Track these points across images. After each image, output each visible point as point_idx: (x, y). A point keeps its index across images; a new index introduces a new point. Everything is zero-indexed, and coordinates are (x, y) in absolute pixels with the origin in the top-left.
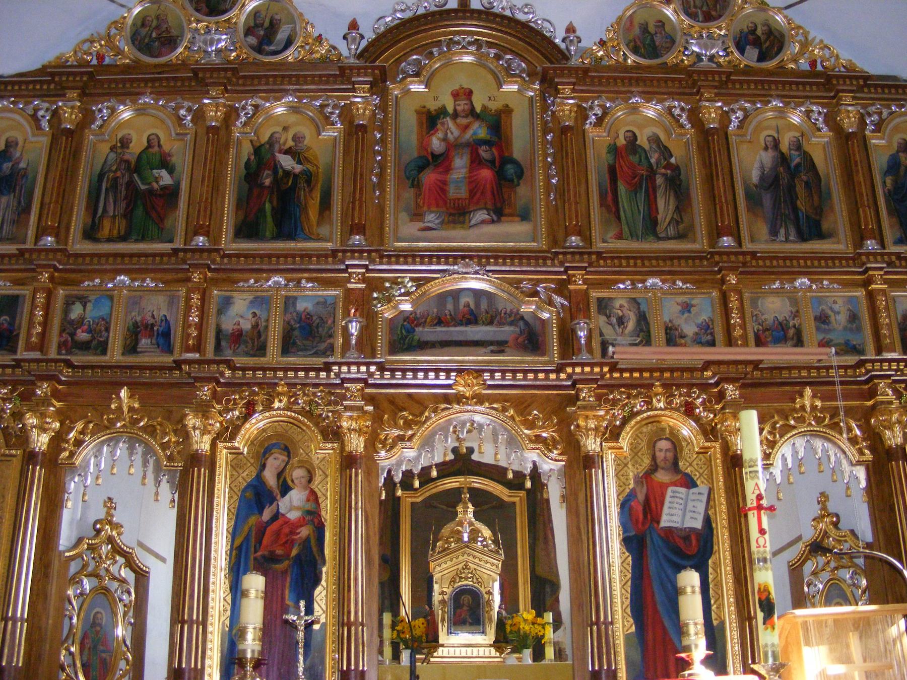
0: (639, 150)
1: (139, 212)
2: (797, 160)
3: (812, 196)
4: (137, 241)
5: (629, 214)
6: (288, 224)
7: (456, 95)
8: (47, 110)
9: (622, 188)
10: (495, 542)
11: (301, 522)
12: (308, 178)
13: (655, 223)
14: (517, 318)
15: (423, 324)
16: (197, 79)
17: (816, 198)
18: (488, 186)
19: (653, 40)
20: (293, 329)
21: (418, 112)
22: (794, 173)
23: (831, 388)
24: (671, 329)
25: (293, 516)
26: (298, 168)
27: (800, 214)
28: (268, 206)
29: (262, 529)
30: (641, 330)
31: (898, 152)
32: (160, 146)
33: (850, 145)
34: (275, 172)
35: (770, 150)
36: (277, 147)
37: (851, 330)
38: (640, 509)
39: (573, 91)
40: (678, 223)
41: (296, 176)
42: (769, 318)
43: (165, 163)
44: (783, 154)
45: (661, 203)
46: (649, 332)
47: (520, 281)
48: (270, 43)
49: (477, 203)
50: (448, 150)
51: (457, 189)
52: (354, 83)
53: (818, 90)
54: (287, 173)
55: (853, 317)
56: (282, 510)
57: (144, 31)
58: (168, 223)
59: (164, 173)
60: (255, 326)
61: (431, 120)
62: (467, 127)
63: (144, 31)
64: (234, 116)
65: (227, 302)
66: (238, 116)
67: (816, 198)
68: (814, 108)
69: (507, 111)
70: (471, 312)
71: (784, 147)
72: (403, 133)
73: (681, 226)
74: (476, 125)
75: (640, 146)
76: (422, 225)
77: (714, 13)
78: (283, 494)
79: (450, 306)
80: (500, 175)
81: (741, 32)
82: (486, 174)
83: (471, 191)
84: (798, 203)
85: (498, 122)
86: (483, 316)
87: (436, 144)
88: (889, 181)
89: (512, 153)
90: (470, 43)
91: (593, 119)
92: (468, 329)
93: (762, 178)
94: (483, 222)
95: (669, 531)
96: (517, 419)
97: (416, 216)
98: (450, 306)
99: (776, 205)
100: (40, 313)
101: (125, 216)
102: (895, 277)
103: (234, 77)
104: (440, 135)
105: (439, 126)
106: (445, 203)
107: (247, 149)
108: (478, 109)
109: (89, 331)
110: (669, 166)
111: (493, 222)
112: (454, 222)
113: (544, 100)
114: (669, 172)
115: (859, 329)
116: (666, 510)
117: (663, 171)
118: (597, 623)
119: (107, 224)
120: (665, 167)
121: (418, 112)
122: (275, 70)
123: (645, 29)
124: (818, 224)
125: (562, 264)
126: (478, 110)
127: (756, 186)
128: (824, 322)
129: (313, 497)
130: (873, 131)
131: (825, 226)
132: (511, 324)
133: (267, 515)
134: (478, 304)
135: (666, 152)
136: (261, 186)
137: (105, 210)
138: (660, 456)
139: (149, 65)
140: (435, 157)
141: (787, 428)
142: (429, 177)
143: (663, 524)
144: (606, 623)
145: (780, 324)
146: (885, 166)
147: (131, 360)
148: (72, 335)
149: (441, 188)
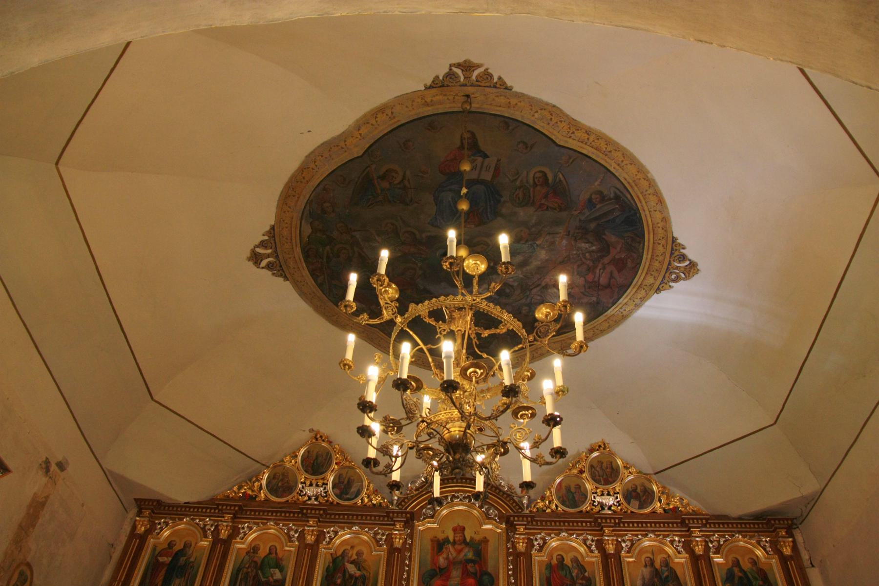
2: (666, 574)
16: (300, 512)
19: (574, 497)
21: (432, 540)
26: (358, 573)
32: (276, 553)
33: (699, 563)
34: (344, 575)
36: (346, 558)
39: (526, 529)
41: (356, 578)
48: (347, 494)
52: (395, 521)
53: (677, 527)
54: (351, 576)
57: (274, 482)
59: (277, 571)
61: (439, 545)
62: (460, 551)
63: (274, 482)
64: (322, 537)
66: (325, 538)
69: (485, 541)
71: (658, 564)
74: (466, 550)
81: (628, 490)
85: (479, 547)
90: (465, 498)
91: (537, 547)
103: (325, 514)
104: (444, 555)
108: (468, 540)
110: (584, 578)
113: (507, 534)
120: (582, 579)
121: (432, 540)
122: (348, 510)
123: (568, 489)
126: (468, 540)
130: (714, 553)
139: (274, 502)
146: (724, 576)
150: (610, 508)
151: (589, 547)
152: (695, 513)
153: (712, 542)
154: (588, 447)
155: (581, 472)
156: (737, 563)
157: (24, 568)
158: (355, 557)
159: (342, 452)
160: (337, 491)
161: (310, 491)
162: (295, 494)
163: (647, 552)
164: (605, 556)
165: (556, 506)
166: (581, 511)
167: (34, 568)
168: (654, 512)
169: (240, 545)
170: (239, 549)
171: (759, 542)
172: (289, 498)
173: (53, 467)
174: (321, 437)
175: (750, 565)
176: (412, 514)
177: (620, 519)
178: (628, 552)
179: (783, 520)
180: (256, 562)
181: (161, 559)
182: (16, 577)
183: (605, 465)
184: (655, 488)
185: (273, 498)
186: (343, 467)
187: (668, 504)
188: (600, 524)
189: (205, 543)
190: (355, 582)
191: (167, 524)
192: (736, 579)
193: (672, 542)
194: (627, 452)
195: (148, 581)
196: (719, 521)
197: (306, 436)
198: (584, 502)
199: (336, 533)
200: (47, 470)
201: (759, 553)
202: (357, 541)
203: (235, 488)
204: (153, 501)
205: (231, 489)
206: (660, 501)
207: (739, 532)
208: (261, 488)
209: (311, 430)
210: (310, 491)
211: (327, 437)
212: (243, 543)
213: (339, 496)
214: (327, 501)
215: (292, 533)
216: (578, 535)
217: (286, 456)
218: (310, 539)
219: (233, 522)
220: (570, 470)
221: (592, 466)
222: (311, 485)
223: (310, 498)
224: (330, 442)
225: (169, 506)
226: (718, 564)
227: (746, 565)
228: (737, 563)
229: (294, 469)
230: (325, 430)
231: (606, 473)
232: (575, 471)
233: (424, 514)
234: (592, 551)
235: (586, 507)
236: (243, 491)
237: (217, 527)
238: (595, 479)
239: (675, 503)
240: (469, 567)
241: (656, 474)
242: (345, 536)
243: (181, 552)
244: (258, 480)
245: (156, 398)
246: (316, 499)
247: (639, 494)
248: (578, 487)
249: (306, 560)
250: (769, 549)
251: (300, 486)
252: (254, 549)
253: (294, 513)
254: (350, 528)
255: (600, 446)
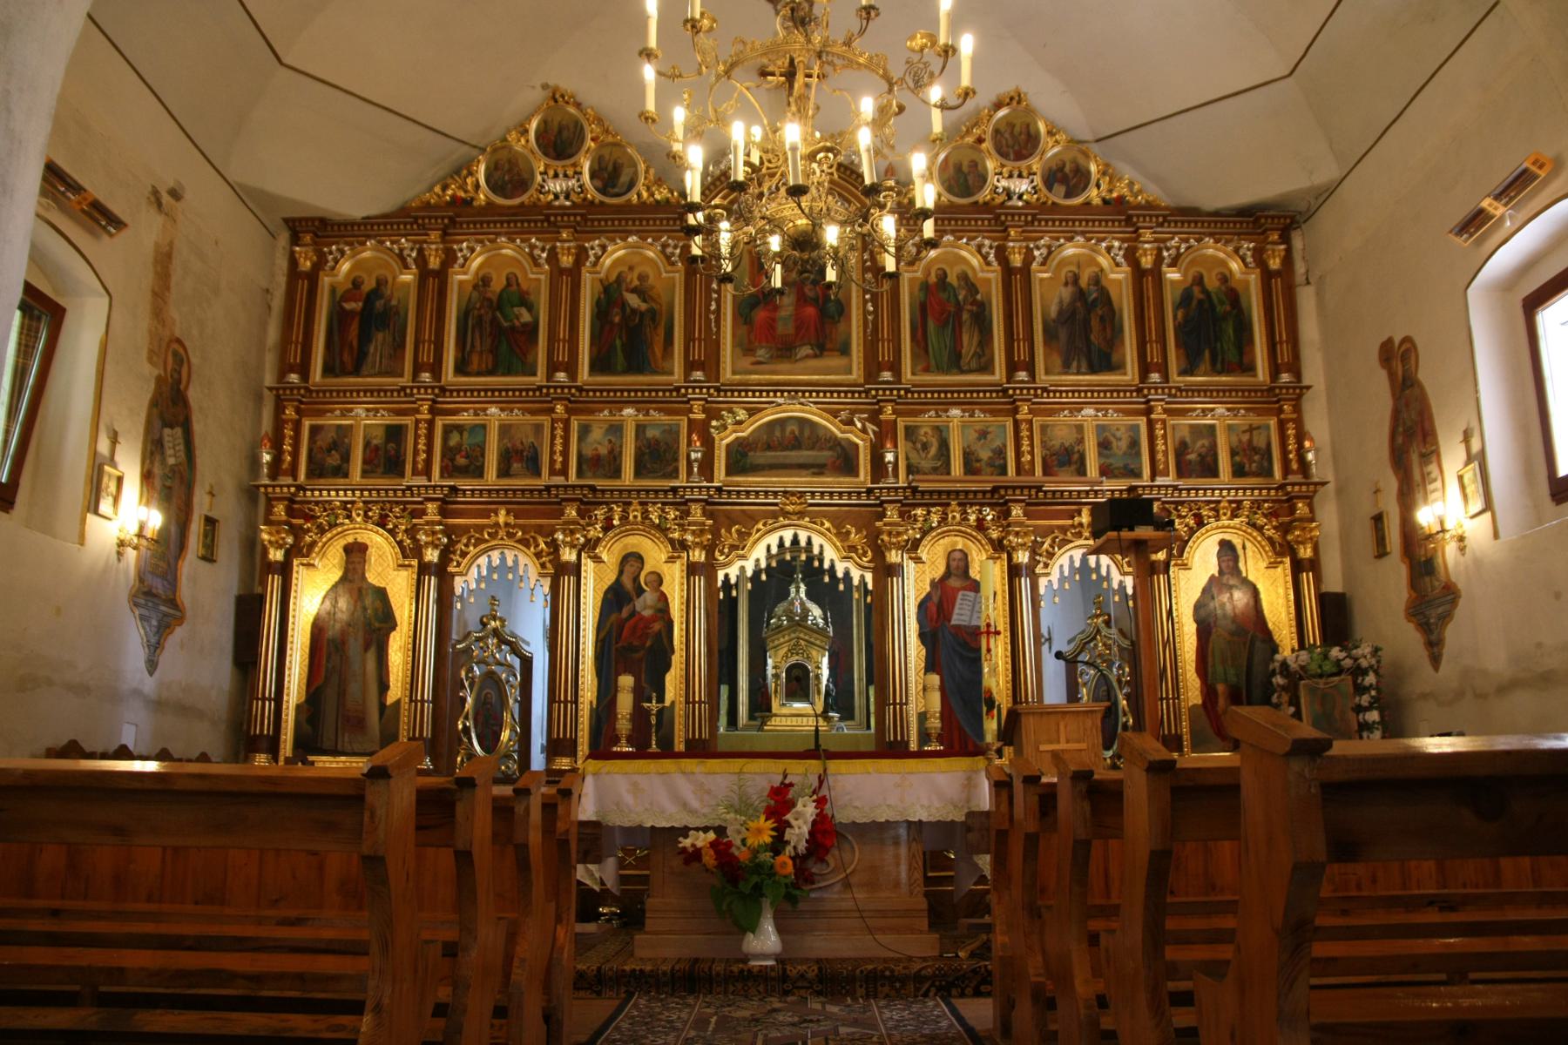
1: (504, 347)
6: (637, 361)
9: (931, 325)
10: (825, 619)
11: (654, 619)
12: (653, 314)
13: (959, 356)
14: (835, 443)
22: (1090, 307)
25: (647, 613)
26: (644, 306)
28: (618, 342)
29: (621, 624)
33: (1145, 280)
38: (934, 609)
41: (642, 314)
43: (525, 301)
45: (965, 338)
47: (839, 411)
48: (614, 186)
51: (785, 327)
54: (634, 311)
56: (638, 608)
57: (497, 175)
58: (530, 358)
59: (524, 311)
60: (611, 452)
65: (585, 431)
66: (588, 257)
70: (796, 438)
71: (1083, 282)
73: (983, 360)
76: (753, 359)
79: (778, 433)
80: (823, 313)
82: (810, 311)
88: (1180, 314)
92: (793, 453)
93: (1060, 313)
94: (807, 356)
95: (958, 627)
98: (778, 433)
100: (422, 441)
103: (588, 219)
109: (467, 457)
110: (975, 302)
111: (816, 356)
116: (956, 611)
118: (895, 704)
119: (475, 359)
123: (958, 168)
131: (1115, 358)
132: (830, 449)
133: (625, 613)
134: (801, 431)
137: (473, 346)
138: (954, 564)
139: (503, 207)
141: (1065, 542)
142: (760, 314)
143: (953, 622)
144: (901, 704)
146: (1178, 300)
147: (506, 483)
148: (452, 460)
149: (771, 324)
150: (1020, 197)
151: (985, 258)
152: (1149, 206)
153: (1168, 249)
154: (994, 99)
155: (980, 140)
156: (1199, 280)
157: (176, 346)
159: (599, 121)
160: (599, 183)
161: (556, 186)
162: (532, 191)
163: (1070, 263)
164: (1008, 271)
166: (976, 203)
167: (187, 344)
168: (1087, 204)
169: (460, 277)
170: (461, 283)
171: (1236, 250)
172: (524, 198)
173: (166, 199)
174: (563, 96)
175: (1217, 284)
177: (1034, 216)
178: (1043, 264)
179: (1279, 218)
180: (489, 300)
181: (348, 306)
182: (170, 360)
183: (1017, 130)
184: (1093, 168)
185: (499, 201)
186: (602, 145)
187: (1110, 191)
188: (1003, 223)
189: (407, 277)
190: (641, 320)
191: (343, 253)
192: (1194, 303)
193: (1109, 249)
194: (1059, 110)
195: (336, 338)
196: (1187, 217)
197: (537, 96)
198: (981, 187)
199: (604, 248)
200: (159, 204)
201: (1235, 266)
202: (636, 259)
203: (437, 189)
204: (313, 219)
205: (430, 189)
206: (1098, 186)
207: (1211, 235)
208: (477, 186)
209: (545, 87)
210: (556, 186)
211: (572, 96)
212: (465, 273)
213: (603, 191)
214: (585, 199)
215: (537, 252)
216: (970, 239)
217: (509, 131)
218: (566, 261)
219: (444, 241)
220: (962, 138)
221: (997, 131)
222: (556, 176)
223: (557, 197)
224: (578, 105)
225: (339, 225)
226: (1173, 282)
227: (1212, 283)
228: (1199, 280)
229: (526, 152)
230: (567, 84)
231: (1017, 142)
232: (970, 140)
234: (988, 264)
235: (984, 195)
236: (450, 192)
237: (421, 251)
238: (1002, 153)
239: (1122, 189)
241: (1098, 141)
242: (616, 252)
243: (376, 293)
244: (470, 173)
245: (286, 60)
246: (567, 197)
247: (1067, 176)
248: (974, 165)
249: (565, 292)
250: (1249, 260)
251: (539, 178)
252: (483, 281)
253: (536, 222)
254: (624, 239)
255: (1012, 99)
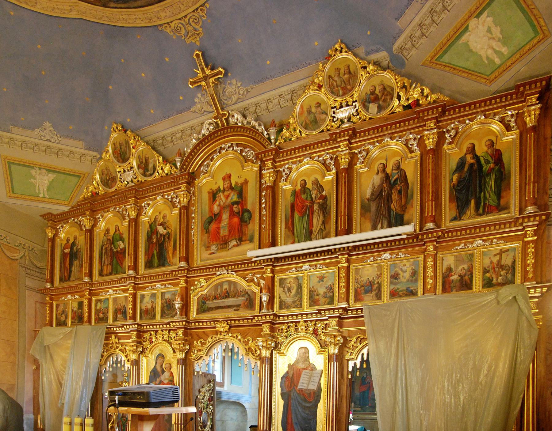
0: (307, 191)
2: (396, 177)
3: (401, 198)
4: (115, 274)
5: (298, 229)
7: (224, 179)
8: (415, 139)
15: (208, 300)
17: (403, 200)
18: (237, 226)
20: (164, 307)
21: (209, 193)
23: (362, 319)
24: (312, 291)
27: (392, 213)
28: (155, 252)
30: (298, 293)
31: (466, 154)
34: (157, 235)
35: (380, 174)
37: (411, 281)
40: (322, 231)
41: (164, 236)
42: (364, 279)
44: (387, 174)
46: (302, 294)
48: (148, 171)
49: (232, 237)
50: (220, 211)
51: (224, 232)
54: (161, 235)
55: (414, 273)
60: (152, 306)
61: (214, 195)
62: (228, 196)
63: (104, 177)
67: (403, 200)
68: (411, 136)
70: (227, 292)
72: (203, 205)
73: (324, 233)
75: (308, 188)
77: (349, 87)
78: (163, 374)
83: (229, 231)
84: (392, 205)
86: (232, 294)
87: (216, 209)
89: (247, 207)
92: (226, 300)
93: (372, 194)
94: (234, 246)
95: (302, 390)
96: (242, 341)
97: (208, 247)
99: (378, 208)
101: (110, 264)
102: (447, 244)
103: (139, 193)
104: (217, 203)
105: (217, 198)
106: (219, 238)
107: (147, 226)
111: (238, 245)
112: (222, 248)
114: (321, 201)
115: (416, 280)
117: (318, 201)
124: (402, 217)
125: (521, 224)
126: (233, 185)
127: (368, 200)
128: (396, 278)
129: (172, 374)
131: (406, 218)
132: (243, 296)
134: (230, 288)
135: (320, 188)
136: (152, 243)
137: (104, 263)
140: (215, 215)
142: (213, 226)
143: (299, 387)
145: (370, 282)
148: (98, 315)
158: (162, 220)
165: (300, 132)
176: (193, 173)
180: (109, 240)
195: (63, 266)
206: (399, 98)
213: (144, 175)
214: (138, 181)
223: (128, 183)
233: (202, 171)
240: (234, 209)
243: (74, 244)
251: (119, 175)
